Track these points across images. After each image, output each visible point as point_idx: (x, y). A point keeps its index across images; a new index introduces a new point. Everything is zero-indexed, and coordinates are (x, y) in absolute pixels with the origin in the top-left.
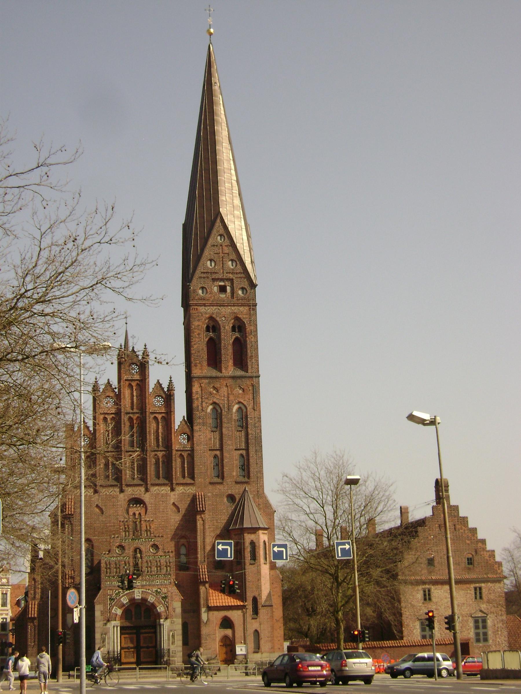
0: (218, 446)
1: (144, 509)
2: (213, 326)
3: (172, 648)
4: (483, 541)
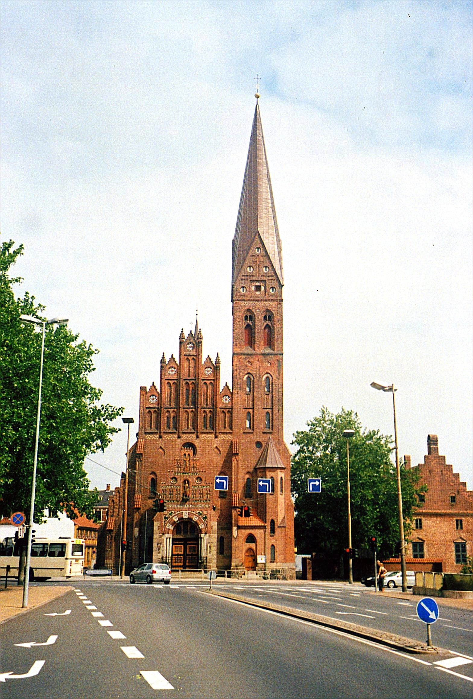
0: (251, 406)
1: (192, 451)
2: (250, 316)
3: (209, 556)
4: (464, 484)
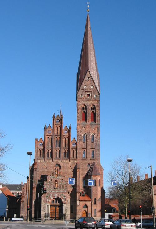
0: (85, 147)
3: (67, 213)
